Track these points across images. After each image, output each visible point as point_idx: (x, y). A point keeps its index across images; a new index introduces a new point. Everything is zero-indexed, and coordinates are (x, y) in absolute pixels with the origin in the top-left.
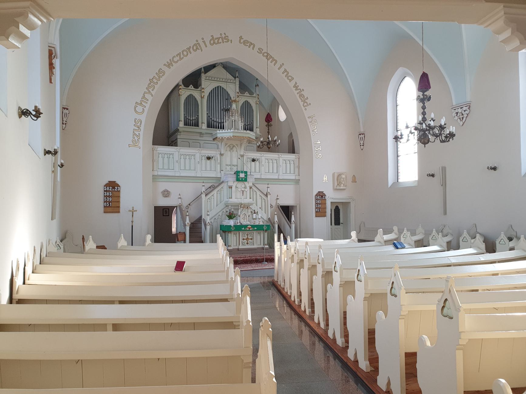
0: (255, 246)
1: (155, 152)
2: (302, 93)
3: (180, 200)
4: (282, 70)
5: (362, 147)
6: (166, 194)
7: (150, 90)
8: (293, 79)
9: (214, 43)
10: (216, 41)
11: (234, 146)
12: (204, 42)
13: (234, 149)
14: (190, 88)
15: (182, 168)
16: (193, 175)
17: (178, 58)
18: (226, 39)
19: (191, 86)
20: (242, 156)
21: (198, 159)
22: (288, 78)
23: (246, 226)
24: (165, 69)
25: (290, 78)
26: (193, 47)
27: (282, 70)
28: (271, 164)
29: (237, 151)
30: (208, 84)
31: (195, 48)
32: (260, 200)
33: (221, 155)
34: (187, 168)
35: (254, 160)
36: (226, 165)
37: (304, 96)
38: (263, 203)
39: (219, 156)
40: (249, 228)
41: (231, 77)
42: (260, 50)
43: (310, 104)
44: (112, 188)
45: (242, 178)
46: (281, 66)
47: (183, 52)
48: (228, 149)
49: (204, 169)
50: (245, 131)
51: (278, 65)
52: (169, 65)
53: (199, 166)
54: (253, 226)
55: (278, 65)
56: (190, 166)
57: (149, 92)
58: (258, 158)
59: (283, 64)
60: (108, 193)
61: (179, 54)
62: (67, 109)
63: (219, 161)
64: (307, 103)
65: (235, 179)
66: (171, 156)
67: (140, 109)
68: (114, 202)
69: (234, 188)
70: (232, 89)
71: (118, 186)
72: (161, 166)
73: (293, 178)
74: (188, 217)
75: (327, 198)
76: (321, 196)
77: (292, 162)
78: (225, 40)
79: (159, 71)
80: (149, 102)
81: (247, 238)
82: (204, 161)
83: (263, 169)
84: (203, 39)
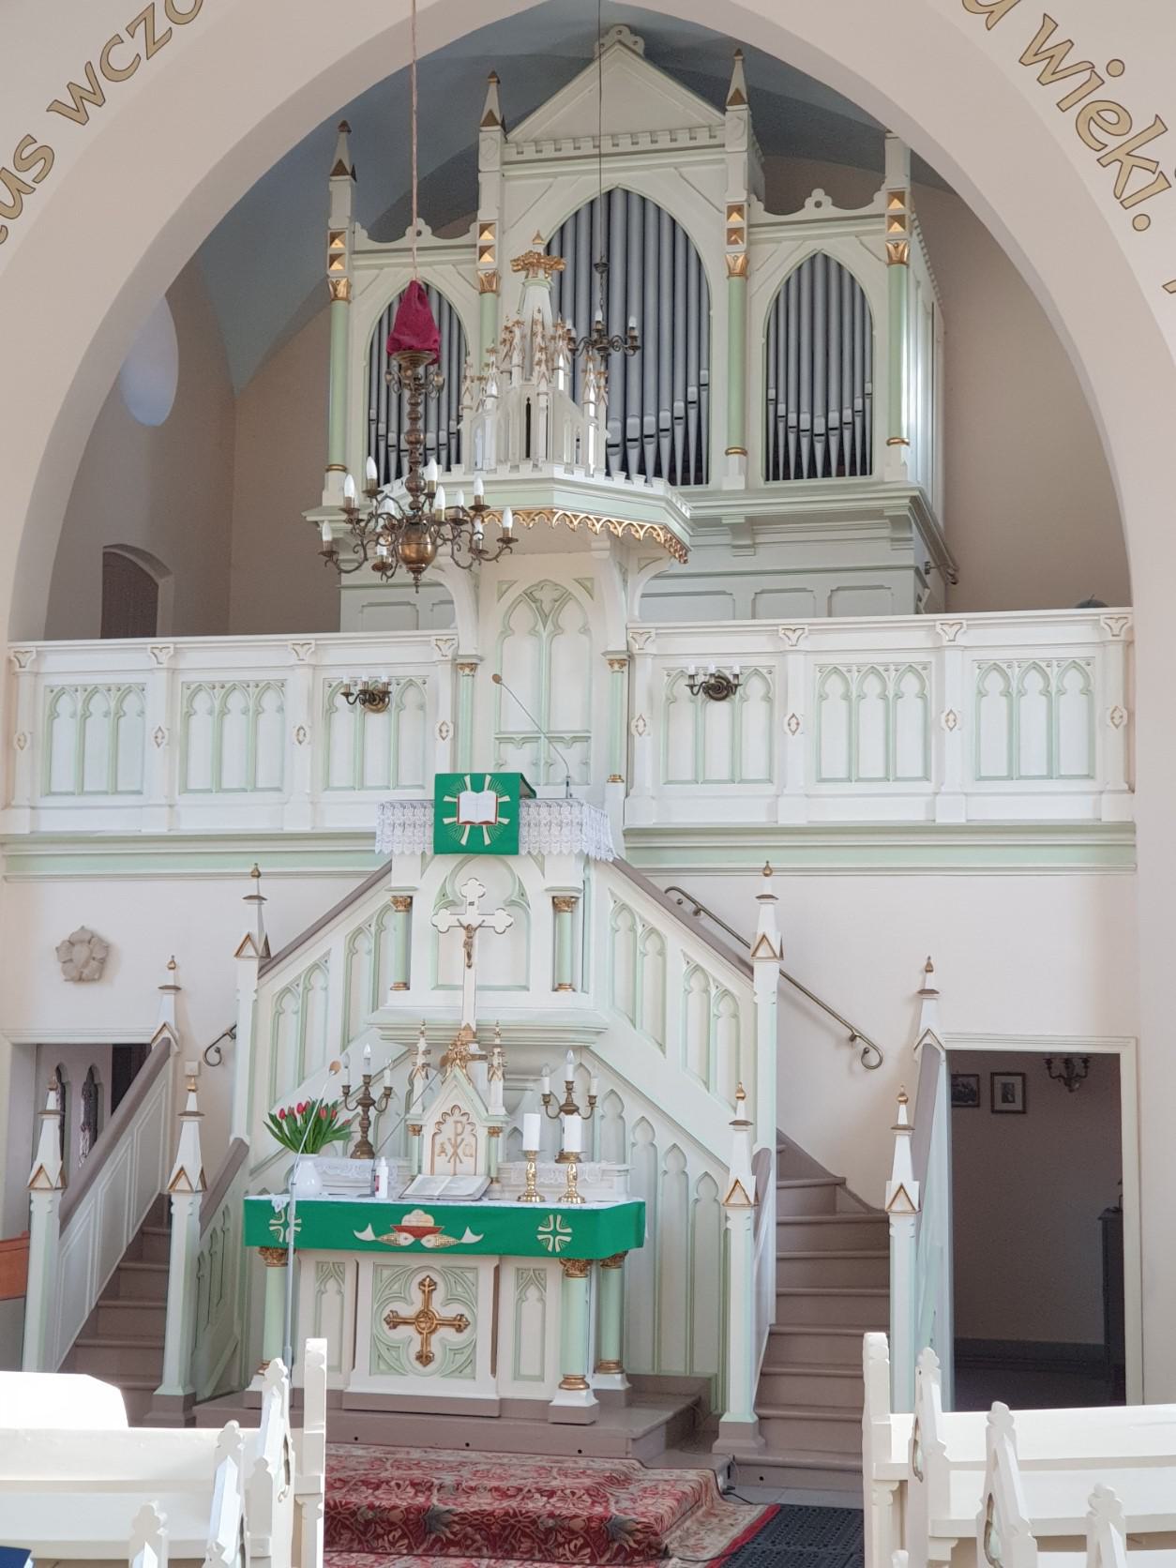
1: (25, 682)
3: (169, 998)
6: (87, 959)
11: (563, 598)
13: (570, 615)
14: (809, 211)
15: (199, 777)
16: (261, 825)
17: (137, 44)
19: (818, 194)
20: (626, 661)
21: (298, 713)
23: (389, 1216)
24: (55, 132)
28: (871, 711)
30: (528, 197)
32: (695, 999)
34: (872, 762)
35: (720, 688)
36: (503, 739)
38: (722, 1030)
39: (443, 677)
40: (419, 1232)
45: (476, 828)
48: (524, 614)
50: (619, 480)
52: (79, 103)
54: (450, 1218)
56: (852, 760)
58: (411, 672)
61: (147, 17)
63: (445, 714)
66: (270, 700)
70: (701, 178)
72: (63, 776)
73: (1069, 805)
77: (1073, 681)
79: (18, 156)
81: (425, 1314)
82: (348, 716)
83: (796, 752)
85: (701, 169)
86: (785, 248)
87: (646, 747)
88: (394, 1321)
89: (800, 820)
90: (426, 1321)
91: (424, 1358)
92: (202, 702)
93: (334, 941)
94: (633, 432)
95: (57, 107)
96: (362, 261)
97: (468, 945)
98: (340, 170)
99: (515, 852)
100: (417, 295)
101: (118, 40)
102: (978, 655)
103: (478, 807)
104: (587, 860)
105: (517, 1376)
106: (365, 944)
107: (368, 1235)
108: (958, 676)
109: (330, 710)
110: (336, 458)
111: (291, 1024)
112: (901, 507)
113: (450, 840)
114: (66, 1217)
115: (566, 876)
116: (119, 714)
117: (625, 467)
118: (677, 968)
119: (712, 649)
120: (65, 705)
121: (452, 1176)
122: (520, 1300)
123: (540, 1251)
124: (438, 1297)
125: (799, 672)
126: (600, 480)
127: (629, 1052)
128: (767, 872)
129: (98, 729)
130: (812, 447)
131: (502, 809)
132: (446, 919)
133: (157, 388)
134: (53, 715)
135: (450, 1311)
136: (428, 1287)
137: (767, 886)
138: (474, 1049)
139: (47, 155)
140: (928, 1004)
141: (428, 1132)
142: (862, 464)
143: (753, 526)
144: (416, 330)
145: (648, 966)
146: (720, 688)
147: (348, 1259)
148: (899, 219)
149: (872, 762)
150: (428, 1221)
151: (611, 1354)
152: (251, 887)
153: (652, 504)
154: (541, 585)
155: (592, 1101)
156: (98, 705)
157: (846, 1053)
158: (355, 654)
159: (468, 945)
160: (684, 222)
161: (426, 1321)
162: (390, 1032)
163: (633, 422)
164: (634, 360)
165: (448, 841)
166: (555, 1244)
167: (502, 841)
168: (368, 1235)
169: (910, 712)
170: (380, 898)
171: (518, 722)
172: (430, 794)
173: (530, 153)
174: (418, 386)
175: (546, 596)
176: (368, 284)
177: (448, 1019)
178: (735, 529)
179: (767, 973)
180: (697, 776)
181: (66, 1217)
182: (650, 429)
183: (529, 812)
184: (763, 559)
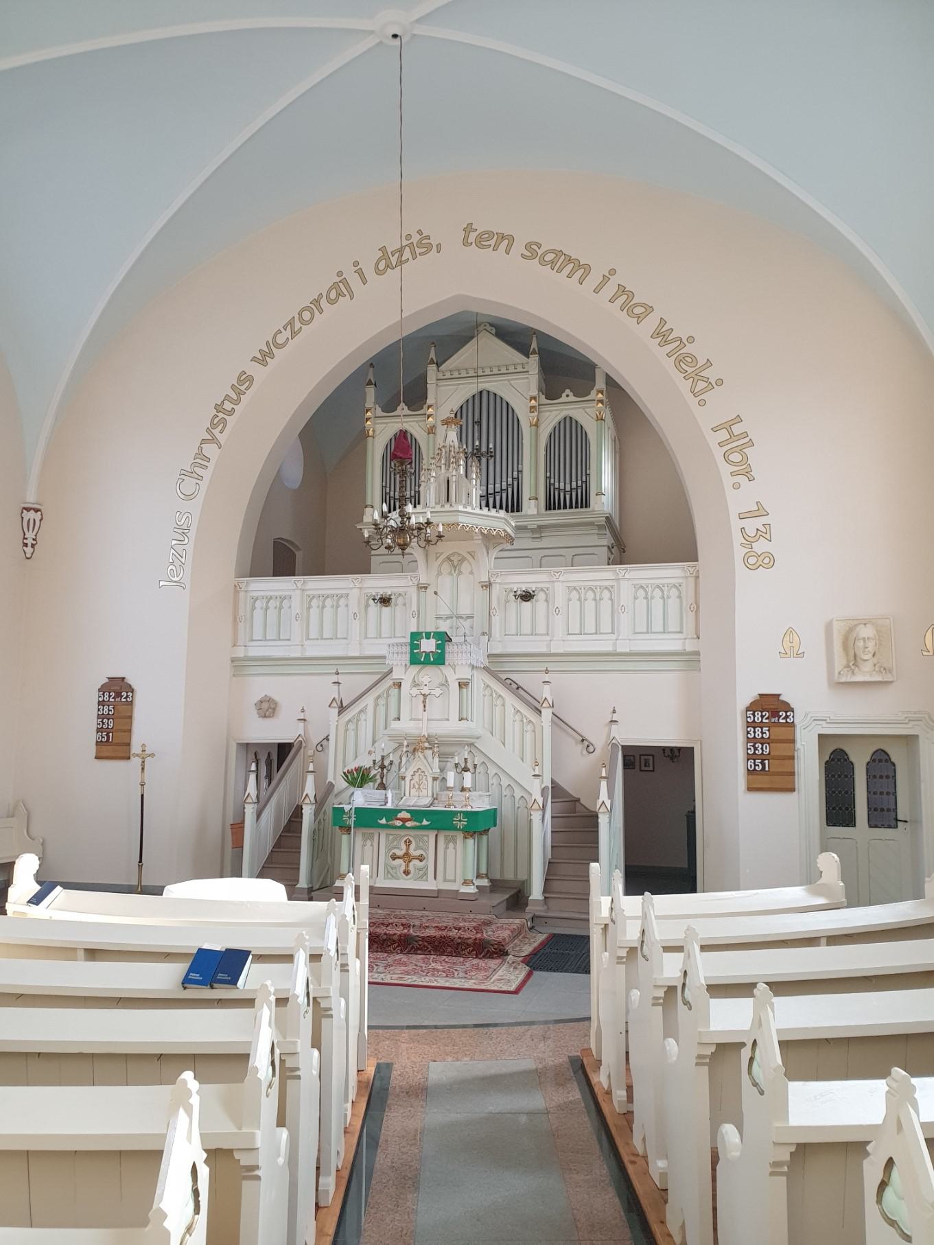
0: (430, 885)
1: (242, 594)
2: (689, 348)
3: (301, 724)
4: (610, 289)
6: (268, 708)
7: (216, 432)
8: (649, 309)
10: (394, 260)
11: (463, 560)
12: (360, 272)
13: (465, 567)
14: (563, 399)
17: (288, 333)
18: (424, 245)
19: (568, 391)
20: (488, 585)
21: (354, 608)
22: (630, 313)
24: (255, 370)
25: (638, 310)
27: (610, 289)
29: (471, 573)
30: (447, 395)
31: (333, 295)
32: (517, 724)
35: (527, 596)
38: (529, 737)
39: (413, 592)
40: (404, 820)
41: (517, 357)
42: (532, 250)
43: (720, 382)
44: (117, 694)
45: (427, 654)
46: (606, 279)
47: (300, 314)
48: (446, 567)
49: (372, 632)
51: (594, 279)
52: (264, 358)
54: (417, 814)
55: (594, 279)
59: (613, 272)
61: (291, 322)
62: (37, 510)
63: (414, 608)
64: (707, 380)
65: (406, 658)
67: (189, 485)
68: (775, 758)
69: (405, 686)
70: (519, 386)
71: (788, 708)
72: (258, 634)
74: (310, 779)
75: (799, 718)
76: (771, 709)
78: (418, 251)
79: (239, 379)
80: (211, 465)
81: (407, 854)
82: (374, 608)
84: (356, 264)
86: (553, 415)
87: (496, 620)
88: (394, 857)
89: (561, 651)
90: (407, 857)
91: (407, 873)
92: (314, 603)
93: (369, 700)
94: (498, 489)
95: (254, 359)
97: (424, 702)
98: (370, 383)
103: (428, 646)
105: (445, 880)
106: (382, 702)
107: (383, 821)
108: (626, 590)
109: (367, 606)
110: (369, 502)
111: (351, 734)
112: (602, 521)
114: (259, 816)
115: (465, 673)
117: (487, 505)
118: (510, 711)
121: (418, 798)
122: (446, 848)
123: (455, 829)
124: (413, 846)
125: (560, 590)
126: (477, 511)
127: (490, 746)
128: (547, 672)
129: (272, 613)
130: (568, 495)
131: (438, 646)
132: (415, 691)
133: (295, 473)
134: (254, 608)
137: (547, 677)
138: (427, 745)
140: (614, 726)
141: (408, 779)
142: (585, 503)
144: (402, 451)
145: (498, 710)
146: (527, 596)
147: (375, 831)
148: (601, 401)
150: (408, 816)
151: (483, 871)
152: (335, 678)
153: (499, 520)
154: (453, 554)
157: (580, 747)
158: (377, 583)
159: (424, 702)
160: (511, 403)
161: (407, 857)
162: (392, 738)
165: (415, 660)
166: (460, 825)
167: (439, 659)
168: (383, 821)
169: (606, 606)
170: (388, 683)
171: (444, 611)
173: (448, 375)
176: (382, 431)
177: (416, 732)
178: (533, 530)
179: (547, 713)
180: (517, 632)
181: (259, 816)
182: (498, 489)
183: (449, 648)
184: (545, 543)
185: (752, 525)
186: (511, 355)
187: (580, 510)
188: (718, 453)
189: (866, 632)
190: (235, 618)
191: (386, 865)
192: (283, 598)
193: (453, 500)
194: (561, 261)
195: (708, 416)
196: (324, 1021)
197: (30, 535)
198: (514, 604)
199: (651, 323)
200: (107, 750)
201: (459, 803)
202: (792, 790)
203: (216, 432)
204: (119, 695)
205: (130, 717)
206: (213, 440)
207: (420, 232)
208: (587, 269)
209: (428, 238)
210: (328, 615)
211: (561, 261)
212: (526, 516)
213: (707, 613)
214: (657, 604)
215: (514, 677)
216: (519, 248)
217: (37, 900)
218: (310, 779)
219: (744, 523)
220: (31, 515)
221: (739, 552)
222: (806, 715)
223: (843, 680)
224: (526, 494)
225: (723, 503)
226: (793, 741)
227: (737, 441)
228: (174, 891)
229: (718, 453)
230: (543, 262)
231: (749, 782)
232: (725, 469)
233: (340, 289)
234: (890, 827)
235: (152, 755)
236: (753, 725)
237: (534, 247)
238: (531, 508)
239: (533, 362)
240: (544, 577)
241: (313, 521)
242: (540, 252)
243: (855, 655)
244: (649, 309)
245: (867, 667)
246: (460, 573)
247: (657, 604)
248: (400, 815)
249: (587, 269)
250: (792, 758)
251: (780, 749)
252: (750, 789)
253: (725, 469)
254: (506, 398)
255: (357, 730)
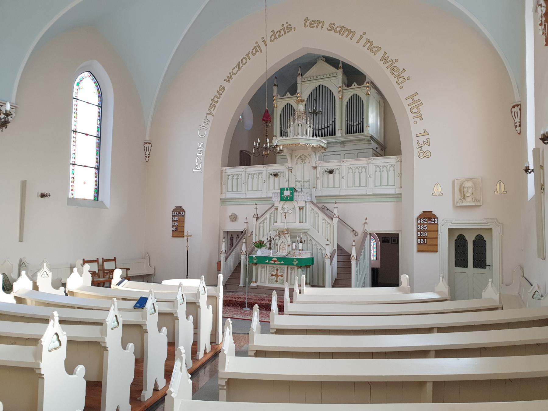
1: (224, 174)
3: (246, 224)
4: (363, 41)
5: (518, 128)
6: (234, 218)
7: (212, 110)
8: (379, 48)
9: (275, 38)
10: (277, 35)
11: (306, 157)
14: (353, 86)
15: (250, 189)
16: (259, 196)
17: (237, 69)
18: (288, 28)
19: (355, 83)
20: (315, 168)
21: (264, 178)
22: (372, 51)
23: (270, 259)
24: (225, 84)
25: (375, 49)
26: (252, 51)
27: (363, 41)
30: (305, 89)
32: (324, 224)
33: (290, 170)
35: (331, 172)
37: (398, 68)
38: (328, 229)
39: (286, 171)
40: (275, 261)
42: (332, 27)
43: (409, 78)
44: (179, 212)
45: (287, 197)
46: (361, 37)
47: (242, 60)
48: (300, 161)
50: (315, 137)
51: (357, 37)
52: (228, 80)
53: (265, 184)
54: (279, 259)
55: (357, 37)
57: (211, 112)
59: (364, 33)
60: (422, 227)
61: (239, 64)
62: (149, 143)
63: (287, 177)
64: (403, 78)
70: (335, 82)
71: (435, 217)
72: (230, 189)
76: (428, 217)
77: (392, 169)
79: (220, 89)
81: (277, 274)
82: (272, 178)
83: (344, 182)
85: (334, 80)
86: (349, 94)
87: (319, 182)
88: (272, 275)
89: (344, 194)
90: (277, 275)
91: (277, 281)
92: (250, 176)
93: (267, 215)
94: (323, 127)
95: (225, 80)
96: (279, 100)
97: (285, 215)
98: (275, 85)
99: (293, 200)
100: (288, 106)
101: (234, 68)
102: (376, 165)
103: (287, 193)
104: (306, 202)
105: (261, 282)
106: (272, 215)
107: (267, 261)
108: (372, 168)
109: (269, 177)
110: (275, 134)
111: (261, 228)
112: (369, 138)
113: (283, 199)
114: (226, 259)
115: (302, 204)
116: (238, 179)
117: (316, 136)
118: (321, 219)
119: (329, 165)
120: (230, 177)
121: (282, 253)
122: (291, 272)
123: (293, 265)
124: (279, 271)
125: (344, 169)
126: (311, 138)
127: (313, 233)
128: (336, 203)
129: (235, 181)
130: (355, 127)
131: (291, 193)
132: (282, 211)
133: (249, 122)
134: (228, 179)
135: (280, 274)
136: (277, 270)
137: (336, 205)
138: (286, 232)
139: (224, 88)
140: (366, 225)
141: (279, 245)
142: (362, 131)
143: (343, 143)
144: (288, 112)
145: (316, 219)
146: (331, 172)
147: (265, 265)
148: (368, 87)
149: (357, 184)
150: (276, 259)
151: (308, 282)
152: (255, 206)
153: (322, 142)
154: (302, 155)
155: (305, 241)
156: (235, 177)
157: (352, 233)
158: (273, 168)
159: (285, 215)
160: (332, 90)
161: (277, 275)
162: (275, 230)
163: (323, 125)
164: (320, 116)
165: (282, 199)
166: (295, 263)
167: (291, 199)
168: (267, 261)
169: (364, 174)
170: (273, 209)
171: (299, 178)
172: (280, 191)
173: (306, 80)
174: (267, 126)
175: (303, 157)
176: (279, 104)
177: (282, 227)
178: (340, 143)
179: (336, 220)
180: (328, 187)
181: (226, 259)
182: (323, 127)
183: (296, 194)
184: (346, 148)
185: (421, 140)
186: (331, 69)
187: (360, 134)
188: (408, 109)
189: (468, 184)
190: (221, 184)
191: (269, 278)
192: (239, 175)
193: (302, 134)
194: (344, 31)
195: (403, 94)
196: (176, 321)
197: (147, 153)
198: (326, 175)
199: (380, 54)
200: (176, 234)
201: (298, 255)
202: (437, 252)
203: (212, 110)
204: (179, 213)
205: (184, 222)
206: (211, 113)
207: (287, 23)
208: (354, 33)
209: (290, 25)
210: (257, 181)
211: (344, 31)
212: (337, 137)
213: (404, 176)
214: (385, 174)
215: (326, 205)
216: (326, 26)
217: (119, 284)
218: (244, 245)
219: (418, 138)
220: (147, 145)
221: (416, 151)
222: (443, 220)
223: (458, 205)
224: (337, 128)
225: (411, 130)
226: (437, 231)
227: (416, 103)
228: (164, 282)
229: (408, 109)
230: (336, 32)
231: (418, 248)
232: (410, 115)
233: (257, 49)
234: (483, 268)
235: (191, 236)
236: (420, 224)
237: (333, 25)
238: (338, 134)
239: (340, 72)
240: (338, 164)
241: (251, 144)
242: (335, 27)
243: (464, 195)
244: (379, 48)
245: (469, 199)
246: (305, 163)
247: (385, 174)
248: (274, 259)
249: (354, 33)
250: (437, 238)
251: (432, 235)
252: (419, 251)
253: (410, 115)
254: (329, 88)
255: (263, 226)
